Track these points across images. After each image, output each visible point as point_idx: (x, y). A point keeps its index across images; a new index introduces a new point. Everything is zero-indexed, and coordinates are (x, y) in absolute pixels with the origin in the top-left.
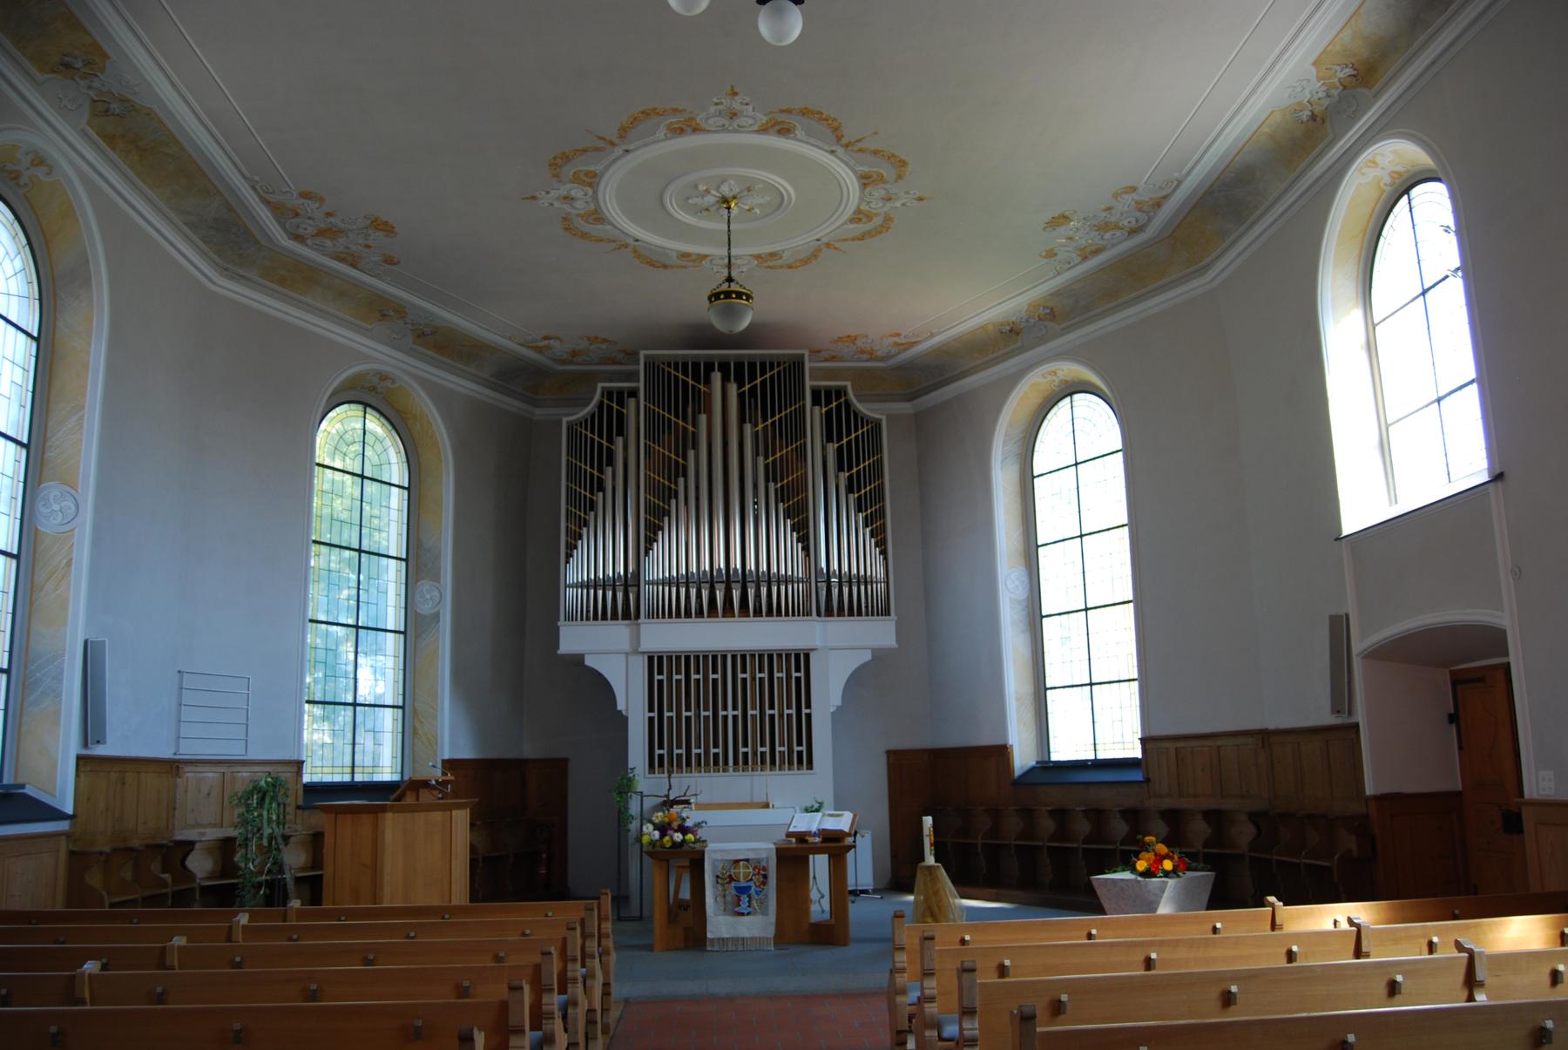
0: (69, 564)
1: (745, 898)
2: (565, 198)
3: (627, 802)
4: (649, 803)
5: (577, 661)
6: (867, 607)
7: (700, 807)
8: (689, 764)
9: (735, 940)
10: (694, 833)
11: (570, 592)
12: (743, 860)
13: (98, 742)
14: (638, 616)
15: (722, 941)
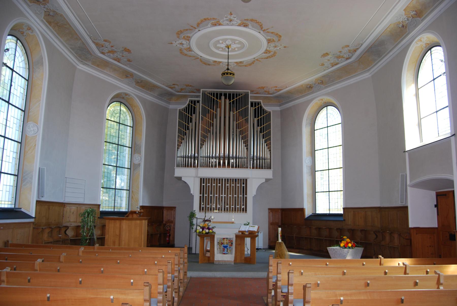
0: (35, 145)
1: (226, 249)
2: (181, 44)
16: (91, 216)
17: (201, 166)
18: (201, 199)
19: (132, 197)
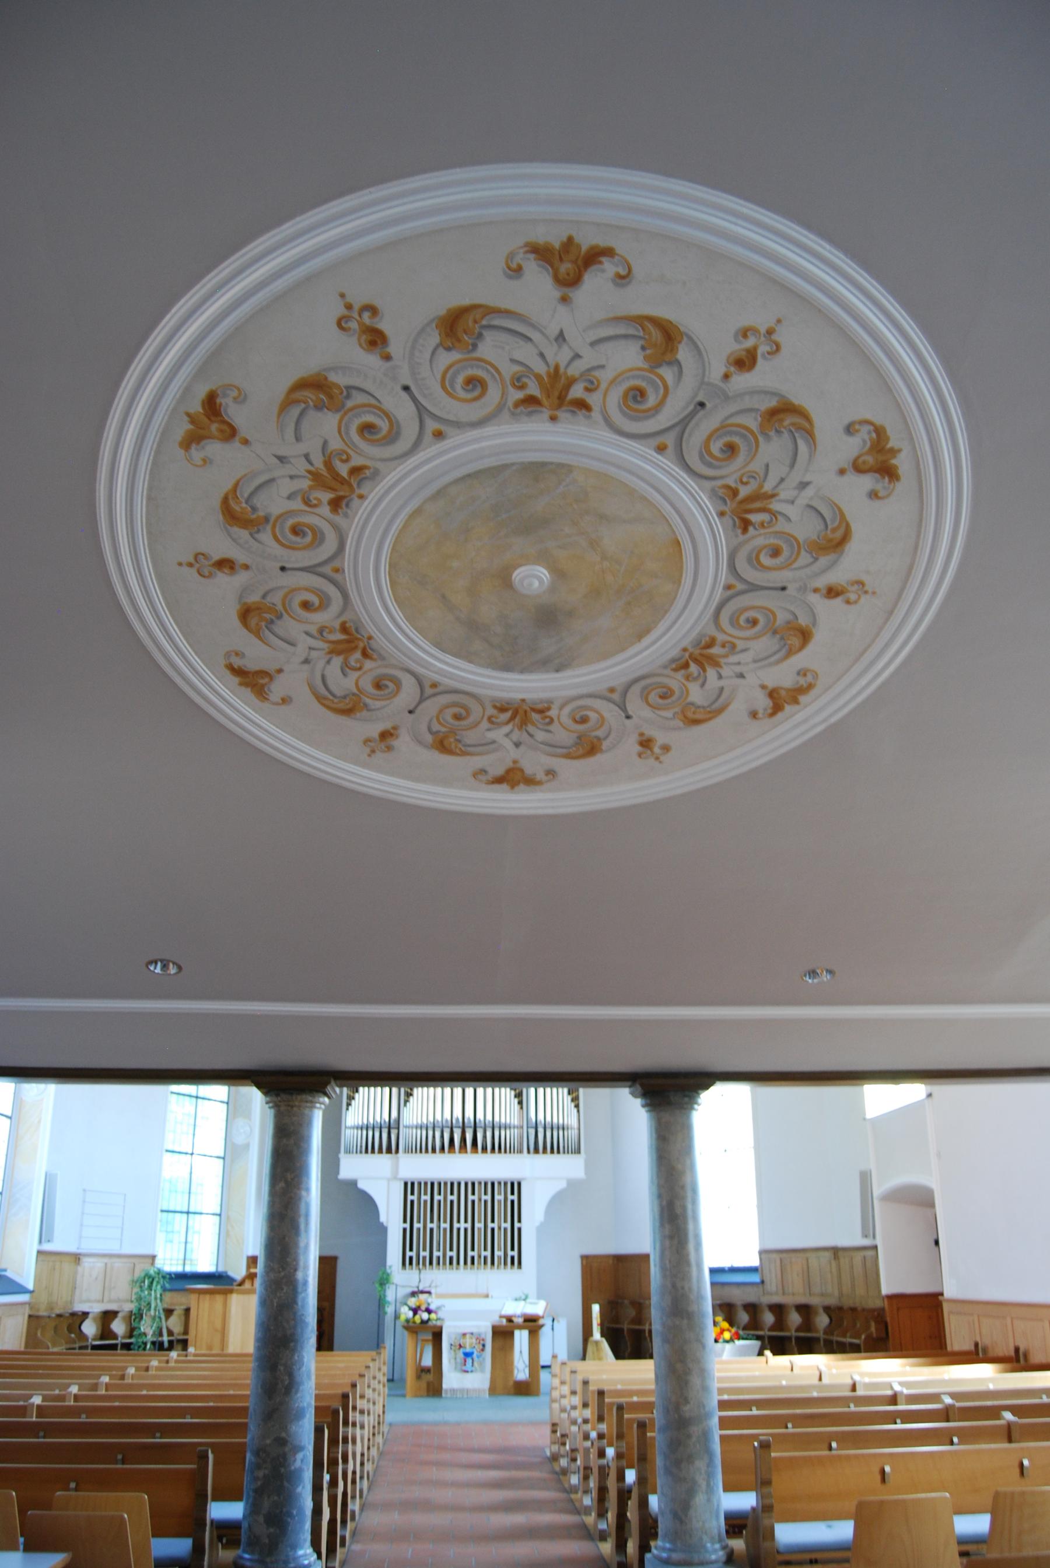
0: (39, 1122)
1: (469, 1360)
3: (385, 1291)
4: (402, 1292)
5: (353, 1184)
6: (564, 1147)
7: (440, 1296)
8: (431, 1263)
9: (462, 1390)
10: (436, 1313)
11: (348, 1132)
12: (622, 257)
13: (49, 1241)
14: (397, 1151)
15: (453, 1391)
16: (156, 1286)
17: (406, 1151)
18: (408, 1239)
19: (228, 1231)
